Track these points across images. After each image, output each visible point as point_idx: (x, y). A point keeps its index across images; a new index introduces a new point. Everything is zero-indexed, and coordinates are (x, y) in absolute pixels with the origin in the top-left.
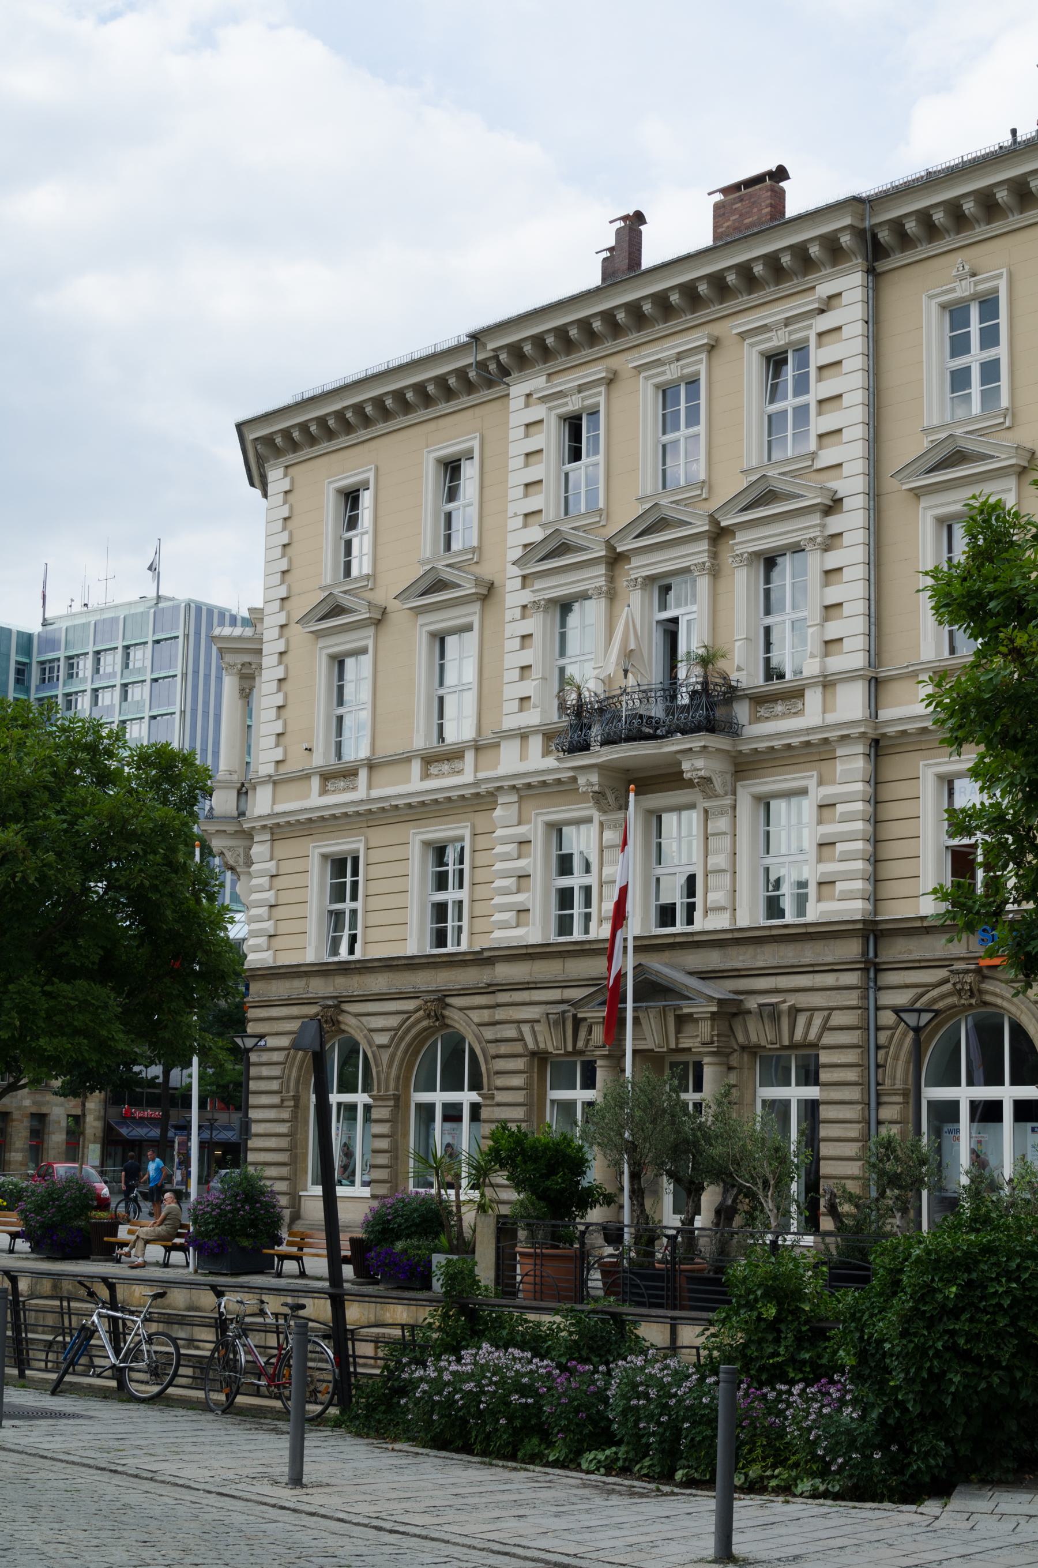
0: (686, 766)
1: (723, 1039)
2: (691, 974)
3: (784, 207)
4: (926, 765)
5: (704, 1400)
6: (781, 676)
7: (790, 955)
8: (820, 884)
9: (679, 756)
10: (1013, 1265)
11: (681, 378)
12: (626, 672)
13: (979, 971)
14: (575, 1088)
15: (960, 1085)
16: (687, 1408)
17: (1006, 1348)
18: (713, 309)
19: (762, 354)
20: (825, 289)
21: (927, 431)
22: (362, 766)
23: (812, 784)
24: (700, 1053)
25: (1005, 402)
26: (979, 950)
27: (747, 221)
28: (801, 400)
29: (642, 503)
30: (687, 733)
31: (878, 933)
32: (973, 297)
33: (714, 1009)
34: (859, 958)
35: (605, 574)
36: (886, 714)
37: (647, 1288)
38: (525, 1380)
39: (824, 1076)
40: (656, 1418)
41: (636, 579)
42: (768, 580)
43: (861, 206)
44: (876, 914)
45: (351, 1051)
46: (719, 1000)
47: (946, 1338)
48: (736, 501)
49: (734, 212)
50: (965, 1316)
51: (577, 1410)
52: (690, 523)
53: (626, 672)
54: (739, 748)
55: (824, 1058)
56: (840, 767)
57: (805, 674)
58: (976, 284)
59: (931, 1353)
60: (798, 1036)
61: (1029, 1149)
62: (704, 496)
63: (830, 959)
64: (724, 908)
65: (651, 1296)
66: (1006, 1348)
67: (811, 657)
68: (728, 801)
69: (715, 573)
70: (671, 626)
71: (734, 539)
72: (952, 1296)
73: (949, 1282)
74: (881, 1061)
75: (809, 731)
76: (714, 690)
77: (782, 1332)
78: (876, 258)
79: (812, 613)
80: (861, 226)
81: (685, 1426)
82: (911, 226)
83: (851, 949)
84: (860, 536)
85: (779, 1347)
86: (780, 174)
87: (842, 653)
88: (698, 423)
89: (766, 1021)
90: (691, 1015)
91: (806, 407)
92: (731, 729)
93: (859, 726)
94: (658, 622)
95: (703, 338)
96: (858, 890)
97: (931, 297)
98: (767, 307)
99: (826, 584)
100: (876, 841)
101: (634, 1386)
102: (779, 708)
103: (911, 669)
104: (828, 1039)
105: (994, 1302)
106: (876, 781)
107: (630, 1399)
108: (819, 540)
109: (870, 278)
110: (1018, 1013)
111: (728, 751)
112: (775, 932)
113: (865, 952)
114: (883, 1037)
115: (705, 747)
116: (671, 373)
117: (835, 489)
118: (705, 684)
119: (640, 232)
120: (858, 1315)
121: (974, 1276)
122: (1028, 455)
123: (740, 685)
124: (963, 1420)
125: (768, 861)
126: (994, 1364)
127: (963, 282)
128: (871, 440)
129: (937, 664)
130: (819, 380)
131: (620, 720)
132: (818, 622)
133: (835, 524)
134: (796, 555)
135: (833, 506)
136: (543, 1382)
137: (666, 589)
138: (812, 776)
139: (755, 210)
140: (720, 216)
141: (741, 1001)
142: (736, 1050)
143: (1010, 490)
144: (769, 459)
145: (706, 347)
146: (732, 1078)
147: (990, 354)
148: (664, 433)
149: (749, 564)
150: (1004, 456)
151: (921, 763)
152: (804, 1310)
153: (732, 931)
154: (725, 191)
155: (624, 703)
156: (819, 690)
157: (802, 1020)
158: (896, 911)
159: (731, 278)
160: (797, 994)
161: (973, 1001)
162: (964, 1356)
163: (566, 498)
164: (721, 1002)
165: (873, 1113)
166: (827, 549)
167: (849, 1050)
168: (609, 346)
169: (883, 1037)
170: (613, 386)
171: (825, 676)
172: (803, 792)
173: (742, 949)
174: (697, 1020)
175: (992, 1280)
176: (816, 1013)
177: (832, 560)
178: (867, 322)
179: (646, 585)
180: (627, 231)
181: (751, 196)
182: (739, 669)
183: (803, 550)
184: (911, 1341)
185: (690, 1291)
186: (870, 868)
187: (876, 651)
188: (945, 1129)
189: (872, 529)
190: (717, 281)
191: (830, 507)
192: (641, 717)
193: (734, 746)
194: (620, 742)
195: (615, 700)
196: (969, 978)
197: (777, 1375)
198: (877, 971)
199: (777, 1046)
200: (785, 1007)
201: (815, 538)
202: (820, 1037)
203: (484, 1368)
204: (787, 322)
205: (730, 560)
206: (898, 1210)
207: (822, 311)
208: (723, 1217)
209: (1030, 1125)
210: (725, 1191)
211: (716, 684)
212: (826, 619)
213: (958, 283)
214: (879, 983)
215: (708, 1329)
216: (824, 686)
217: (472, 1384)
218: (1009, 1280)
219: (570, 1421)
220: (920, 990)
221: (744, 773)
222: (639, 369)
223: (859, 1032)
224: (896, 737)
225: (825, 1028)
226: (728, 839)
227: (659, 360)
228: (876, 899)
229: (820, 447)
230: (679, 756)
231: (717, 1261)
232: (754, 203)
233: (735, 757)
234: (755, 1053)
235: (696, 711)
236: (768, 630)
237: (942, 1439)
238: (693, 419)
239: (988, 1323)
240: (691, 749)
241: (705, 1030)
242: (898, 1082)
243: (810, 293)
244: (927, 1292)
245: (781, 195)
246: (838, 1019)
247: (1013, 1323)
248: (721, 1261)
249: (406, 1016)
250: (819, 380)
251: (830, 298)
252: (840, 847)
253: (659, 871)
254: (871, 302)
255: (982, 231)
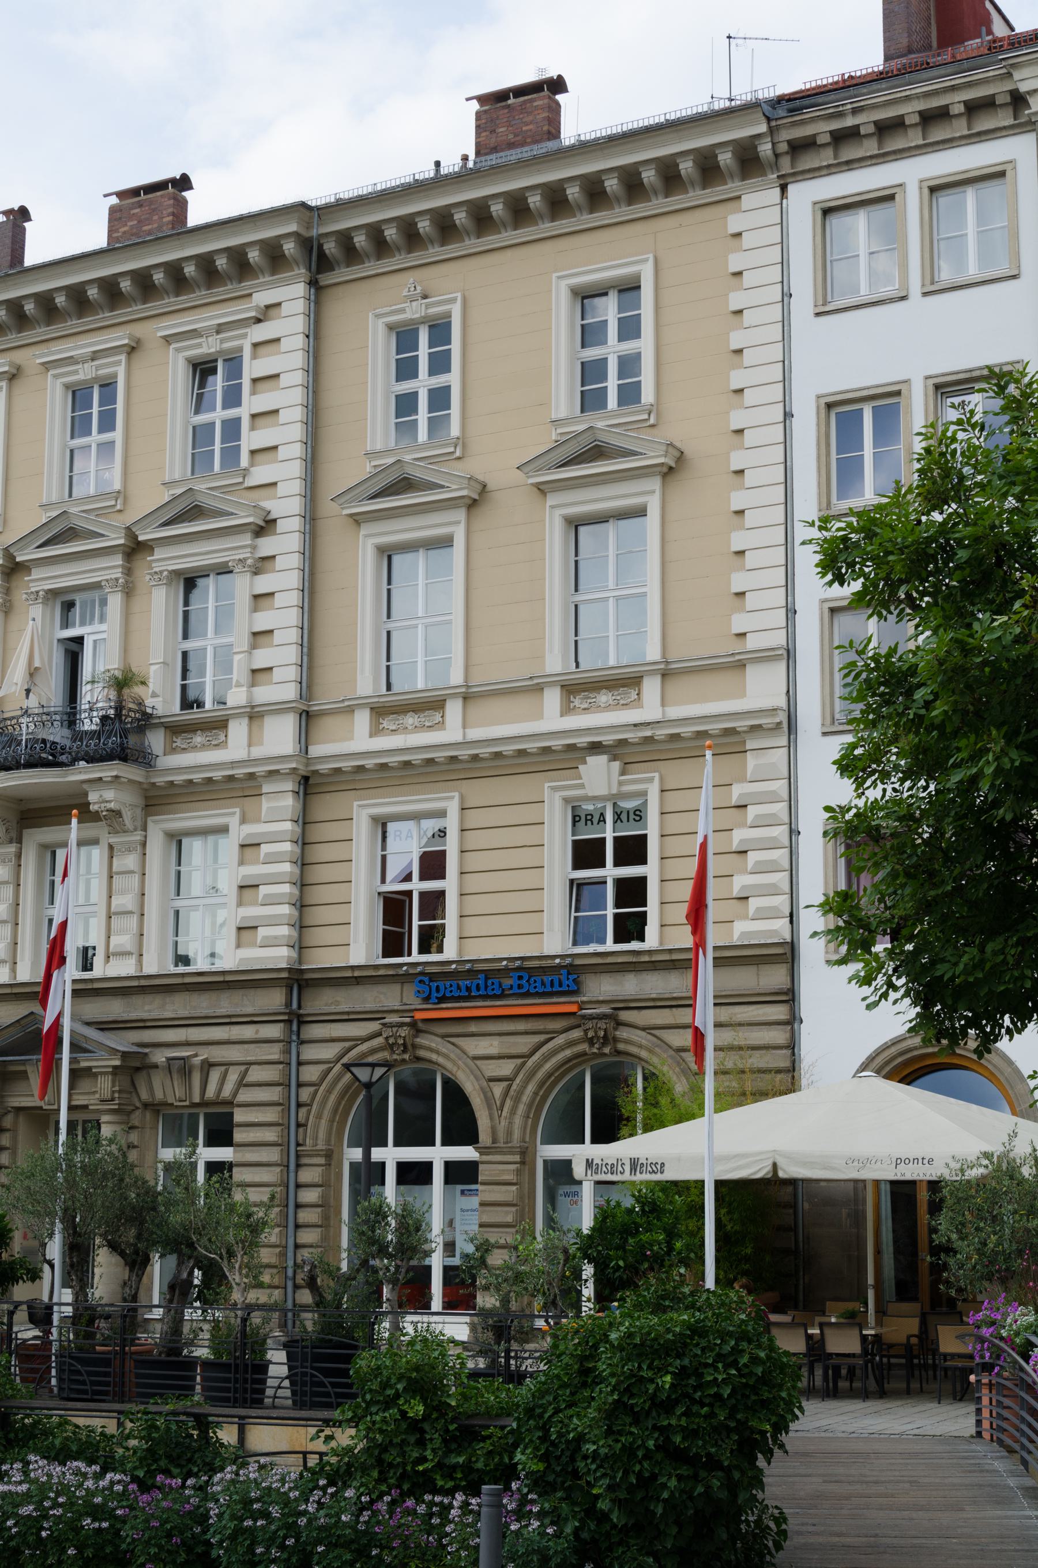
0: (93, 797)
1: (124, 1095)
2: (88, 1024)
3: (186, 218)
4: (360, 806)
5: (343, 1518)
6: (200, 704)
7: (204, 1004)
8: (239, 929)
9: (85, 786)
10: (727, 1348)
11: (96, 379)
12: (28, 691)
13: (413, 1025)
14: (433, 1144)
15: (583, 1143)
16: (321, 1528)
17: (724, 1446)
18: (135, 308)
19: (189, 360)
20: (262, 298)
21: (370, 455)
22: (454, 696)
23: (234, 822)
24: (98, 1111)
25: (455, 431)
26: (415, 1002)
27: (145, 228)
28: (232, 413)
29: (46, 511)
30: (92, 762)
31: (303, 983)
32: (423, 321)
33: (117, 1063)
34: (282, 1009)
35: (123, 566)
36: (316, 750)
37: (89, 1374)
38: (98, 1500)
39: (238, 1136)
40: (279, 1540)
41: (37, 592)
42: (186, 603)
43: (308, 213)
44: (300, 963)
45: (455, 1095)
46: (124, 1052)
47: (656, 1435)
48: (159, 513)
49: (131, 217)
50: (680, 1410)
51: (169, 1535)
52: (103, 535)
53: (28, 691)
54: (153, 781)
55: (239, 1116)
56: (266, 804)
57: (230, 704)
58: (427, 307)
59: (640, 1454)
60: (211, 1092)
61: (458, 1213)
62: (118, 507)
63: (249, 1010)
64: (130, 953)
65: (93, 1383)
66: (724, 1446)
67: (152, 697)
68: (138, 837)
69: (129, 591)
70: (74, 647)
71: (30, 575)
72: (667, 1386)
73: (662, 1370)
74: (302, 1120)
75: (233, 764)
76: (127, 716)
77: (425, 1432)
78: (319, 271)
79: (239, 639)
80: (305, 233)
81: (320, 1549)
82: (360, 240)
83: (274, 1000)
84: (295, 560)
85: (425, 1450)
86: (184, 183)
87: (271, 683)
88: (113, 428)
89: (175, 1076)
90: (90, 1068)
91: (237, 421)
92: (143, 759)
93: (291, 762)
94: (59, 640)
95: (123, 338)
96: (284, 936)
97: (378, 316)
98: (197, 311)
99: (255, 609)
100: (303, 884)
101: (247, 1502)
102: (198, 739)
103: (347, 703)
104: (244, 1096)
105: (712, 1392)
106: (305, 820)
107: (242, 1520)
108: (249, 562)
109: (312, 290)
110: (455, 1069)
111: (140, 782)
112: (187, 980)
113: (288, 1003)
114: (305, 1094)
115: (117, 777)
116: (85, 372)
117: (268, 509)
118: (119, 708)
119: (24, 229)
120: (538, 1411)
121: (686, 1362)
122: (479, 487)
123: (155, 712)
124: (674, 1530)
125: (178, 904)
126: (713, 1464)
127: (414, 304)
128: (309, 460)
129: (376, 700)
130: (253, 392)
131: (19, 744)
132: (246, 649)
133: (267, 546)
134: (220, 577)
135: (266, 527)
136: (119, 1502)
137: (69, 606)
138: (234, 813)
139: (155, 218)
140: (115, 220)
141: (146, 1054)
142: (137, 1108)
143: (459, 522)
144: (70, 495)
145: (125, 349)
146: (134, 1137)
147: (629, 347)
148: (72, 437)
149: (168, 584)
150: (454, 487)
151: (356, 803)
152: (449, 1405)
153: (11, 986)
154: (120, 195)
155: (24, 726)
156: (245, 721)
157: (215, 1075)
158: (322, 959)
159: (158, 277)
160: (210, 1047)
161: (406, 1056)
162: (678, 1456)
163: (71, 477)
164: (125, 1055)
165: (292, 1175)
166: (257, 572)
167: (268, 1108)
168: (138, 309)
169: (305, 1094)
170: (15, 382)
171: (253, 707)
172: (224, 830)
173: (148, 998)
174: (95, 1075)
175: (706, 1365)
176: (232, 1068)
177: (264, 584)
178: (308, 336)
179: (48, 599)
180: (10, 225)
181: (151, 202)
182: (154, 695)
183: (231, 572)
184: (617, 1441)
185: (138, 1376)
186: (296, 913)
187: (308, 684)
188: (561, 1192)
189: (307, 554)
190: (110, 288)
191: (262, 528)
192: (44, 741)
193: (147, 777)
194: (18, 768)
195: (14, 721)
196: (404, 1032)
197: (421, 1485)
198: (301, 1023)
199: (187, 1103)
200: (197, 1061)
201: (245, 559)
202: (235, 1093)
203: (43, 1489)
204: (220, 329)
205: (148, 577)
206: (389, 1282)
207: (259, 321)
208: (177, 1292)
209: (459, 1187)
210: (180, 1264)
211: (130, 710)
212: (254, 646)
213: (408, 304)
214: (302, 1036)
215: (323, 1431)
216: (251, 718)
217: (31, 1508)
218: (726, 1367)
219: (161, 1547)
220: (347, 1044)
221: (169, 807)
222: (47, 366)
223: (280, 1088)
224: (328, 775)
225: (241, 1084)
226: (136, 879)
227: (72, 357)
228: (301, 947)
229: (252, 464)
230: (85, 786)
231: (170, 1341)
232: (154, 210)
233: (146, 790)
234: (158, 1111)
235: (109, 737)
236: (185, 655)
237: (648, 1554)
238: (107, 422)
239: (706, 1417)
240: (100, 779)
241: (105, 1086)
242: (320, 1142)
243: (246, 300)
244: (632, 1385)
245: (183, 205)
246: (256, 1074)
247: (731, 1416)
248: (175, 1341)
249: (542, 1038)
250: (253, 392)
251: (268, 307)
252: (263, 890)
253: (178, 904)
254: (312, 316)
255: (435, 252)
